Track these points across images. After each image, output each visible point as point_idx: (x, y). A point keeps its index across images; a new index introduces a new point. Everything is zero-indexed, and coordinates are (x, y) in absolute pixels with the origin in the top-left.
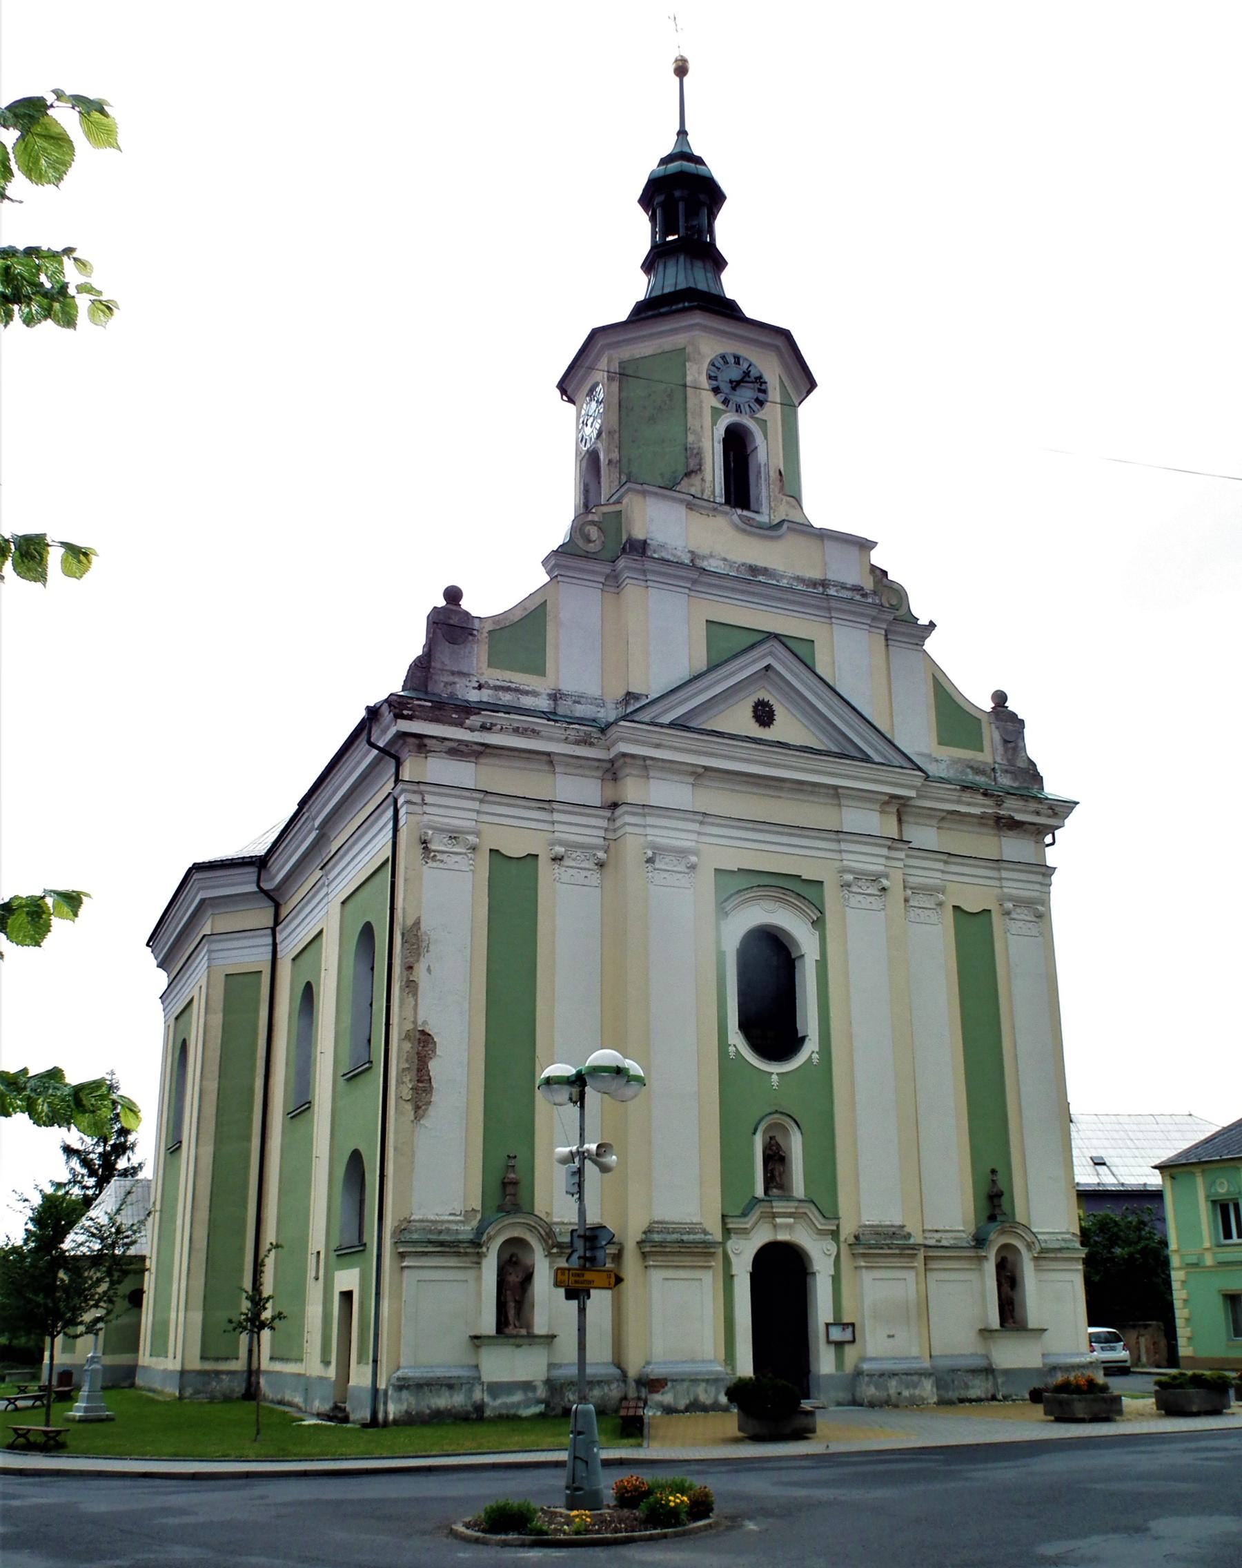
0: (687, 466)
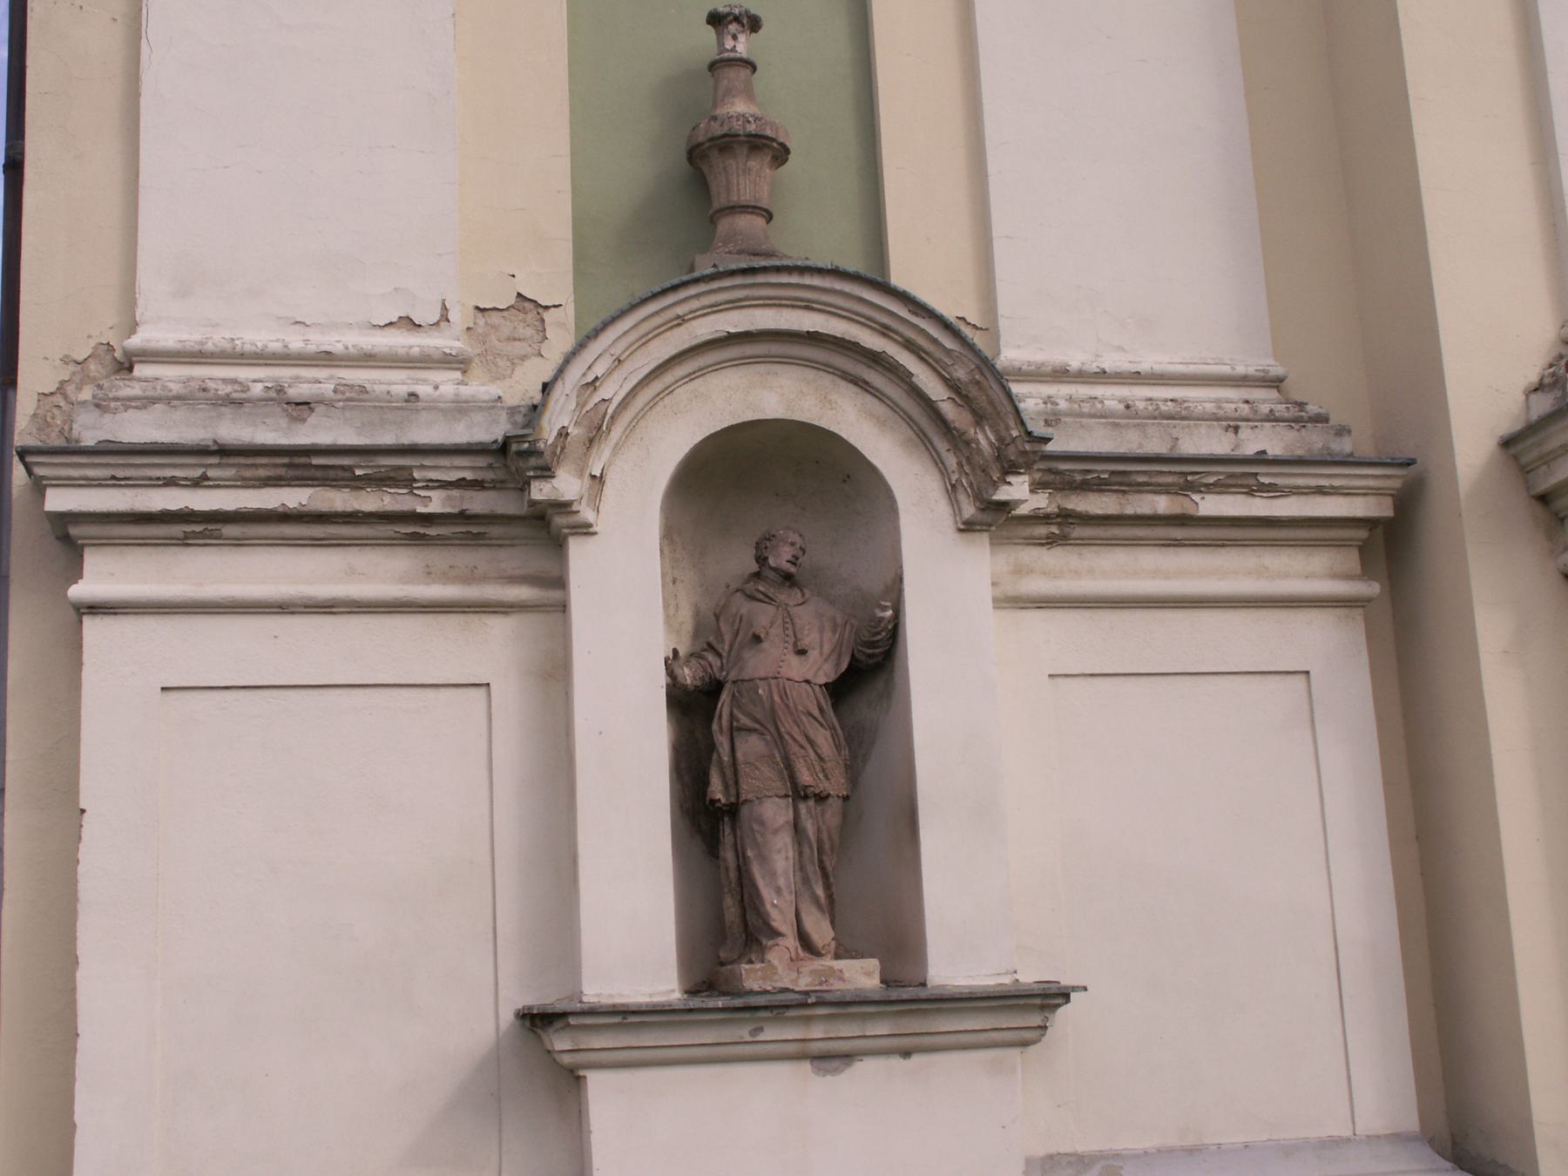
0: (822, 810)
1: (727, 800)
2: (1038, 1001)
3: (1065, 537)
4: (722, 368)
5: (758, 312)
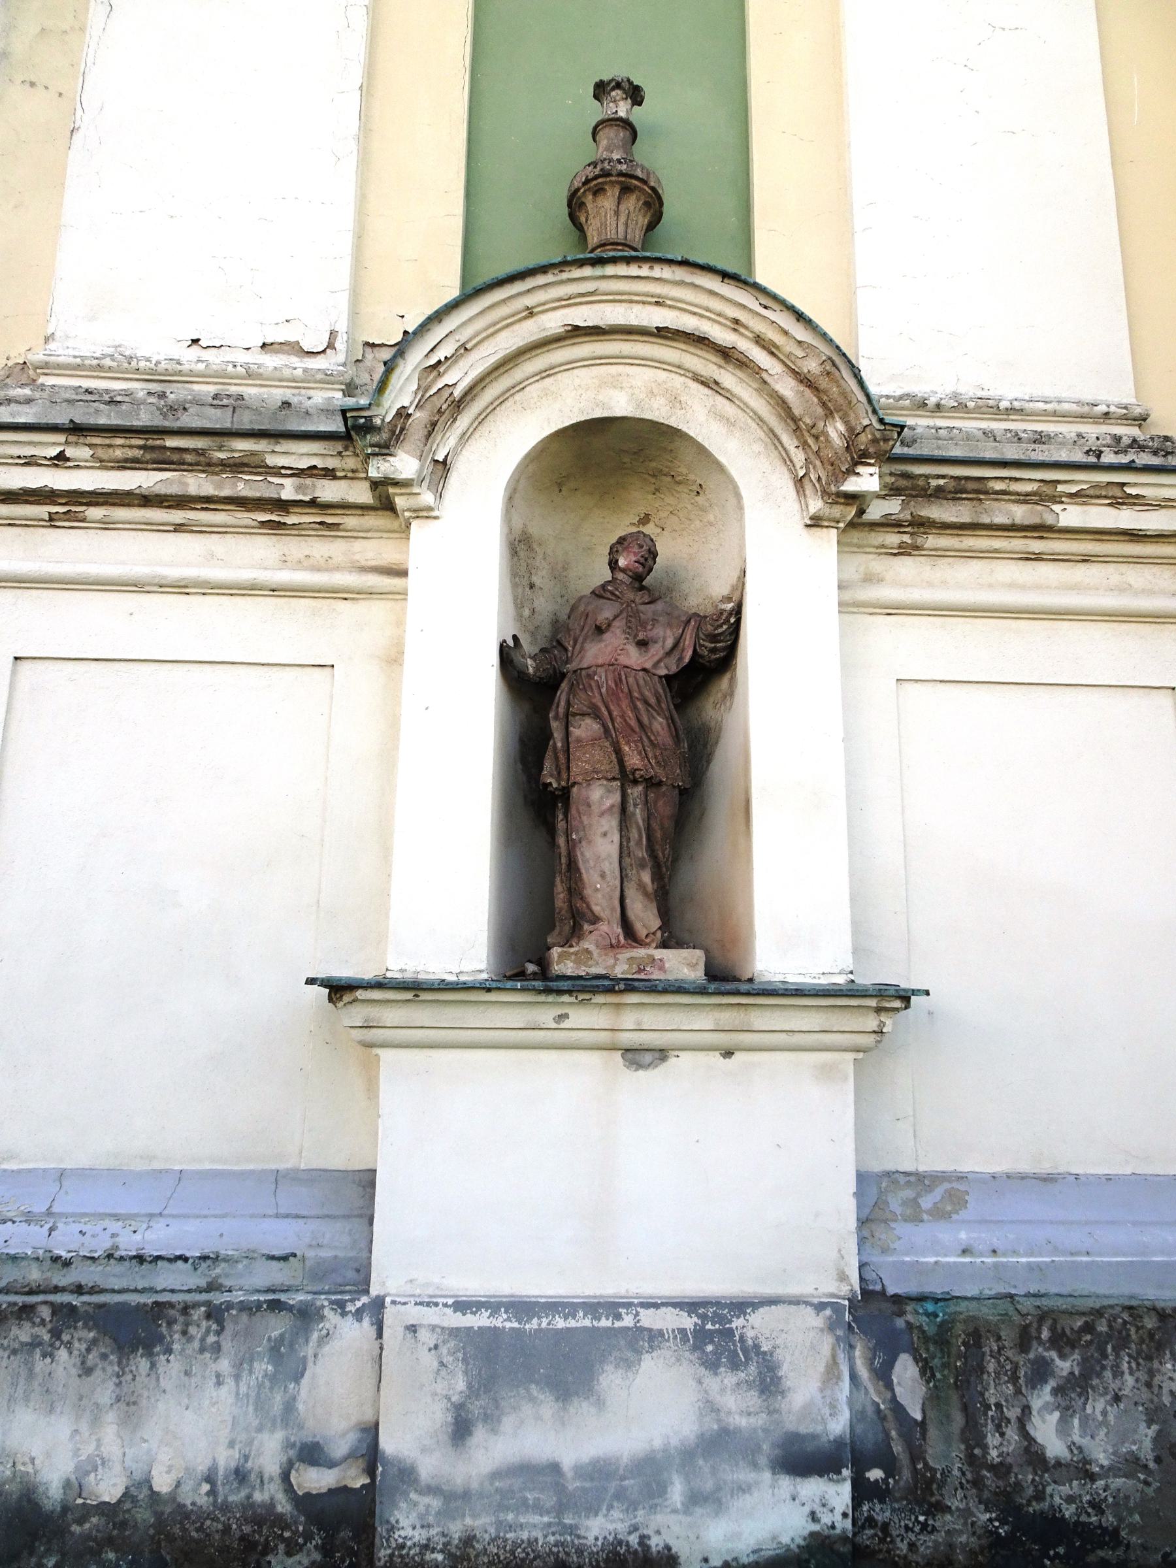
1: (559, 784)
2: (873, 1003)
3: (917, 547)
4: (573, 368)
5: (608, 308)
